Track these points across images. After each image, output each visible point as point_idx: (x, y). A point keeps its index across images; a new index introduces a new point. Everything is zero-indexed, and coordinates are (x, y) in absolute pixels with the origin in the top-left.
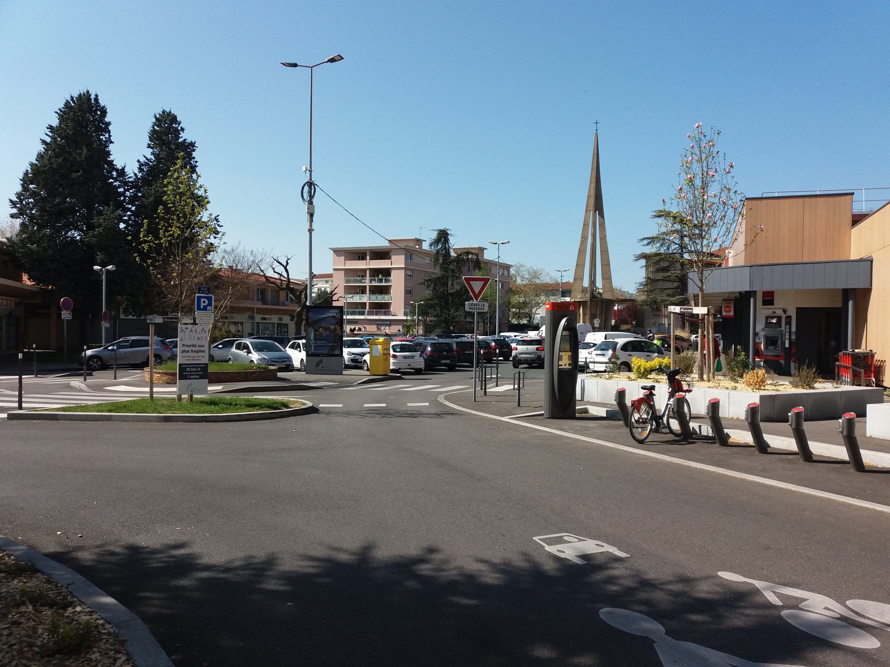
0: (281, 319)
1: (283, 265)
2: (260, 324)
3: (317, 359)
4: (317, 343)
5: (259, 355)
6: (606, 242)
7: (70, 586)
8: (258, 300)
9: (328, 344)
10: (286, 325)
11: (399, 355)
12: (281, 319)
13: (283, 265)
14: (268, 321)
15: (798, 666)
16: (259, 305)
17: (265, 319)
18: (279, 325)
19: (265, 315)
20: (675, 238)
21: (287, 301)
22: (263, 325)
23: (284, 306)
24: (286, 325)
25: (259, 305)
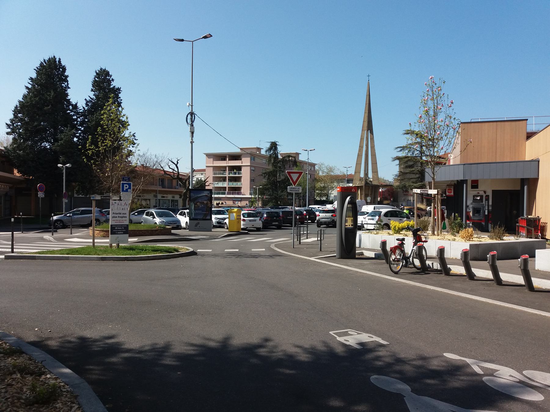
0: (173, 197)
1: (175, 164)
2: (161, 200)
3: (196, 222)
4: (196, 212)
5: (160, 219)
6: (375, 150)
7: (43, 362)
8: (159, 185)
9: (203, 213)
10: (177, 201)
11: (246, 220)
12: (173, 197)
13: (175, 164)
14: (166, 198)
15: (493, 411)
16: (160, 188)
17: (164, 197)
18: (172, 201)
19: (164, 194)
20: (417, 147)
21: (177, 186)
22: (163, 200)
23: (176, 189)
24: (177, 201)
25: (160, 188)
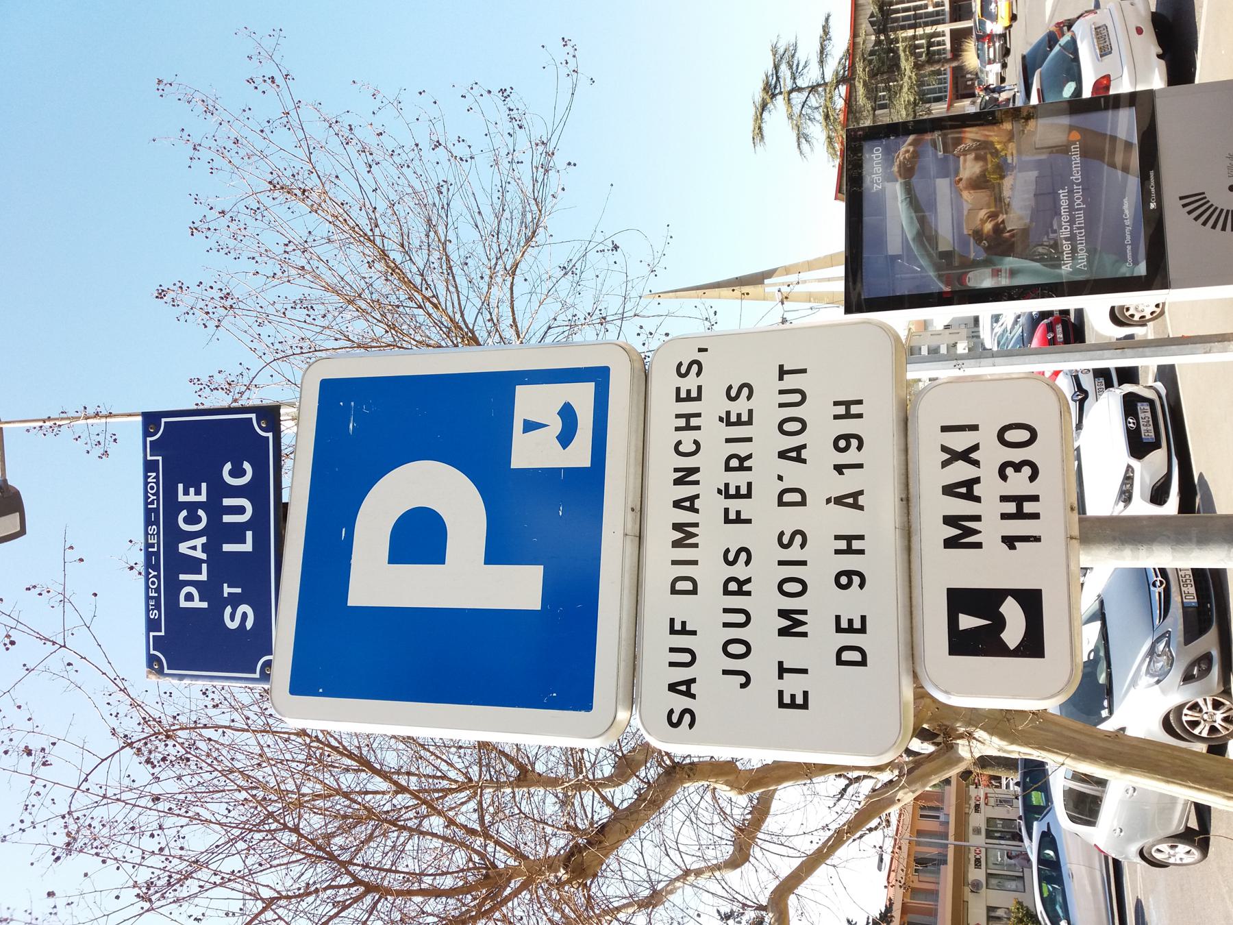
0: (977, 831)
1: (847, 786)
2: (989, 871)
3: (1178, 225)
4: (1072, 238)
5: (1134, 683)
6: (815, 260)
7: (728, 850)
8: (938, 872)
9: (1077, 176)
10: (989, 820)
11: (1096, 70)
12: (977, 831)
13: (847, 786)
14: (983, 855)
15: (1231, 606)
16: (948, 871)
17: (978, 861)
18: (989, 835)
19: (969, 859)
20: (797, 98)
21: (937, 817)
22: (990, 865)
23: (948, 823)
24: (989, 820)
25: (948, 871)
